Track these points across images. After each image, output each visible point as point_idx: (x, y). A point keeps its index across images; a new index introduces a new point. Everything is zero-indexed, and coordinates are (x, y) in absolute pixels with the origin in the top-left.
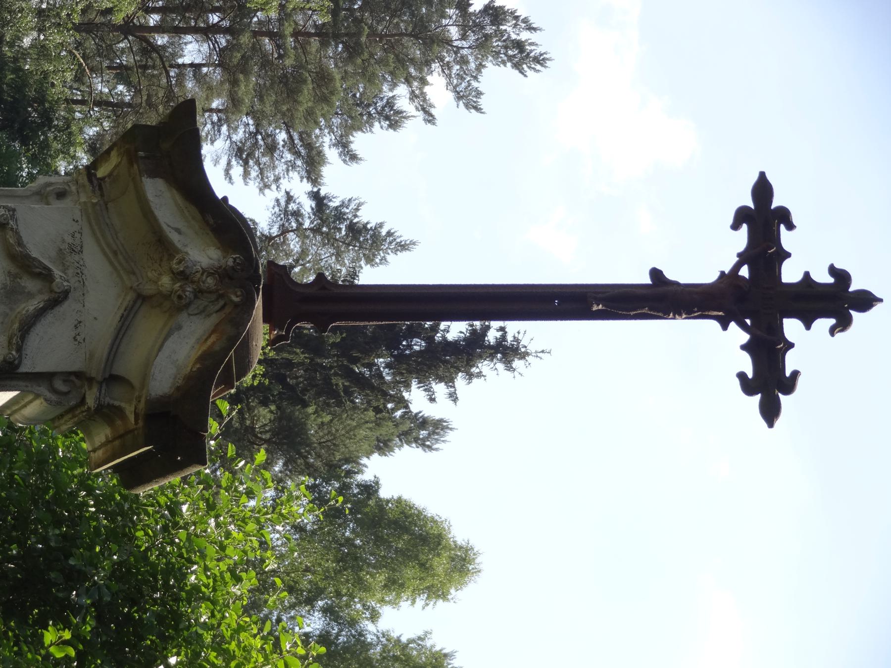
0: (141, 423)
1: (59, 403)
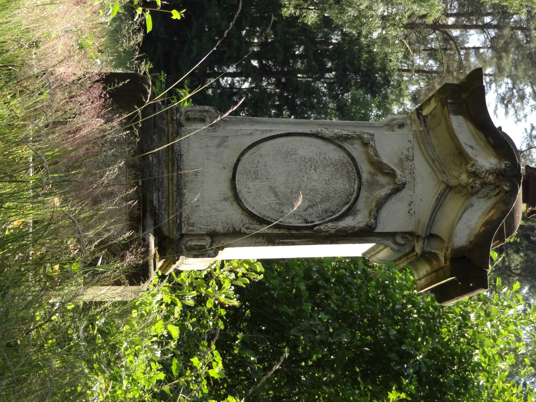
0: (448, 263)
1: (399, 251)
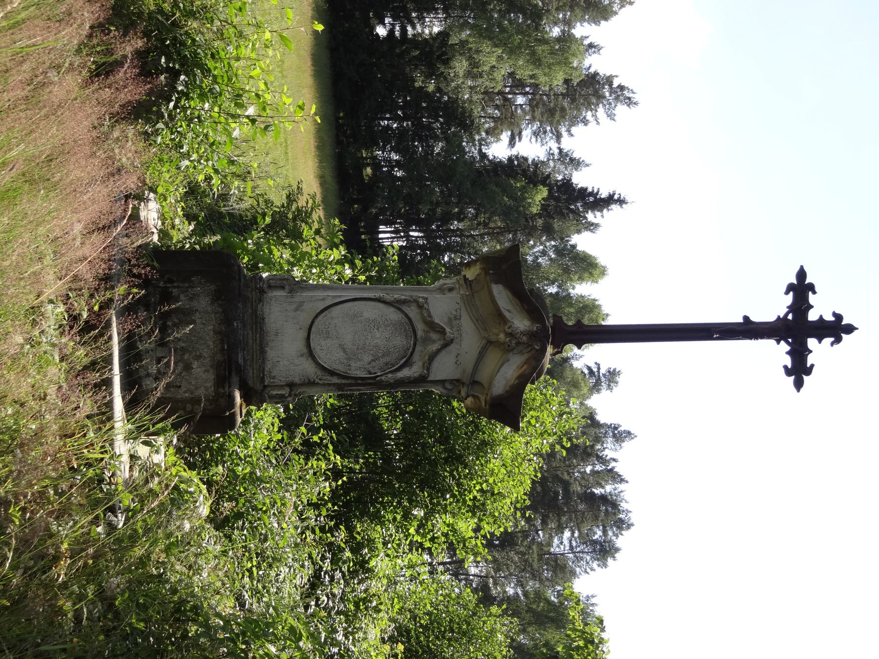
0: (488, 407)
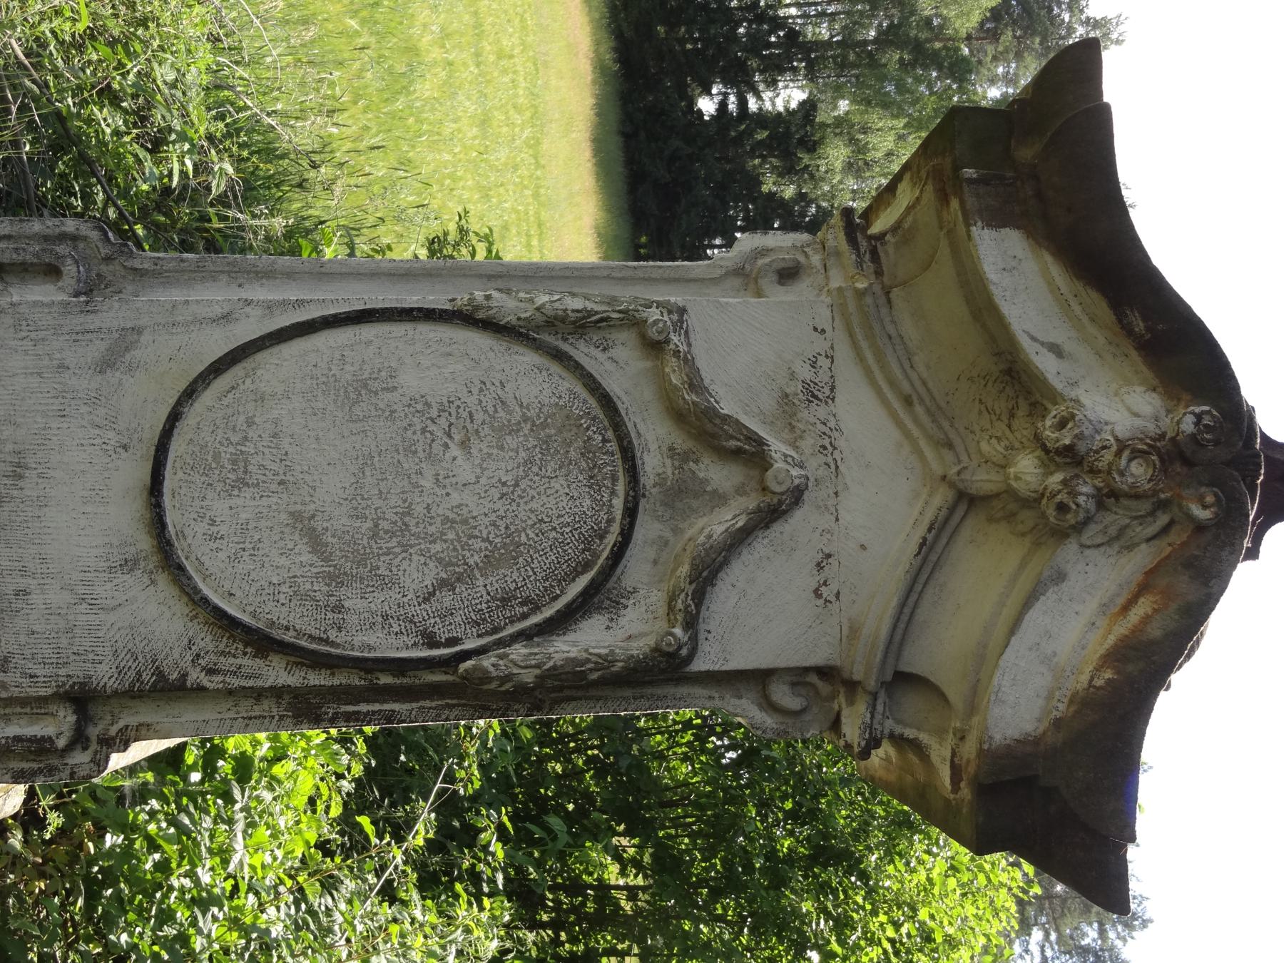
0: (966, 792)
